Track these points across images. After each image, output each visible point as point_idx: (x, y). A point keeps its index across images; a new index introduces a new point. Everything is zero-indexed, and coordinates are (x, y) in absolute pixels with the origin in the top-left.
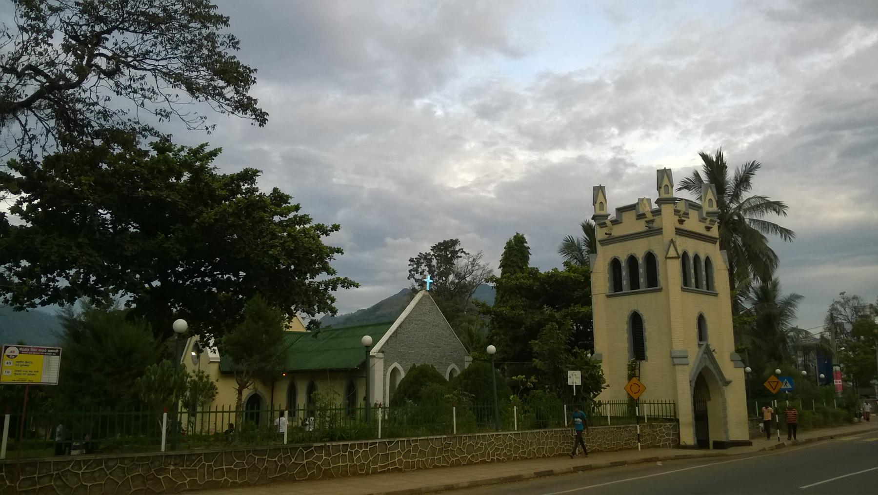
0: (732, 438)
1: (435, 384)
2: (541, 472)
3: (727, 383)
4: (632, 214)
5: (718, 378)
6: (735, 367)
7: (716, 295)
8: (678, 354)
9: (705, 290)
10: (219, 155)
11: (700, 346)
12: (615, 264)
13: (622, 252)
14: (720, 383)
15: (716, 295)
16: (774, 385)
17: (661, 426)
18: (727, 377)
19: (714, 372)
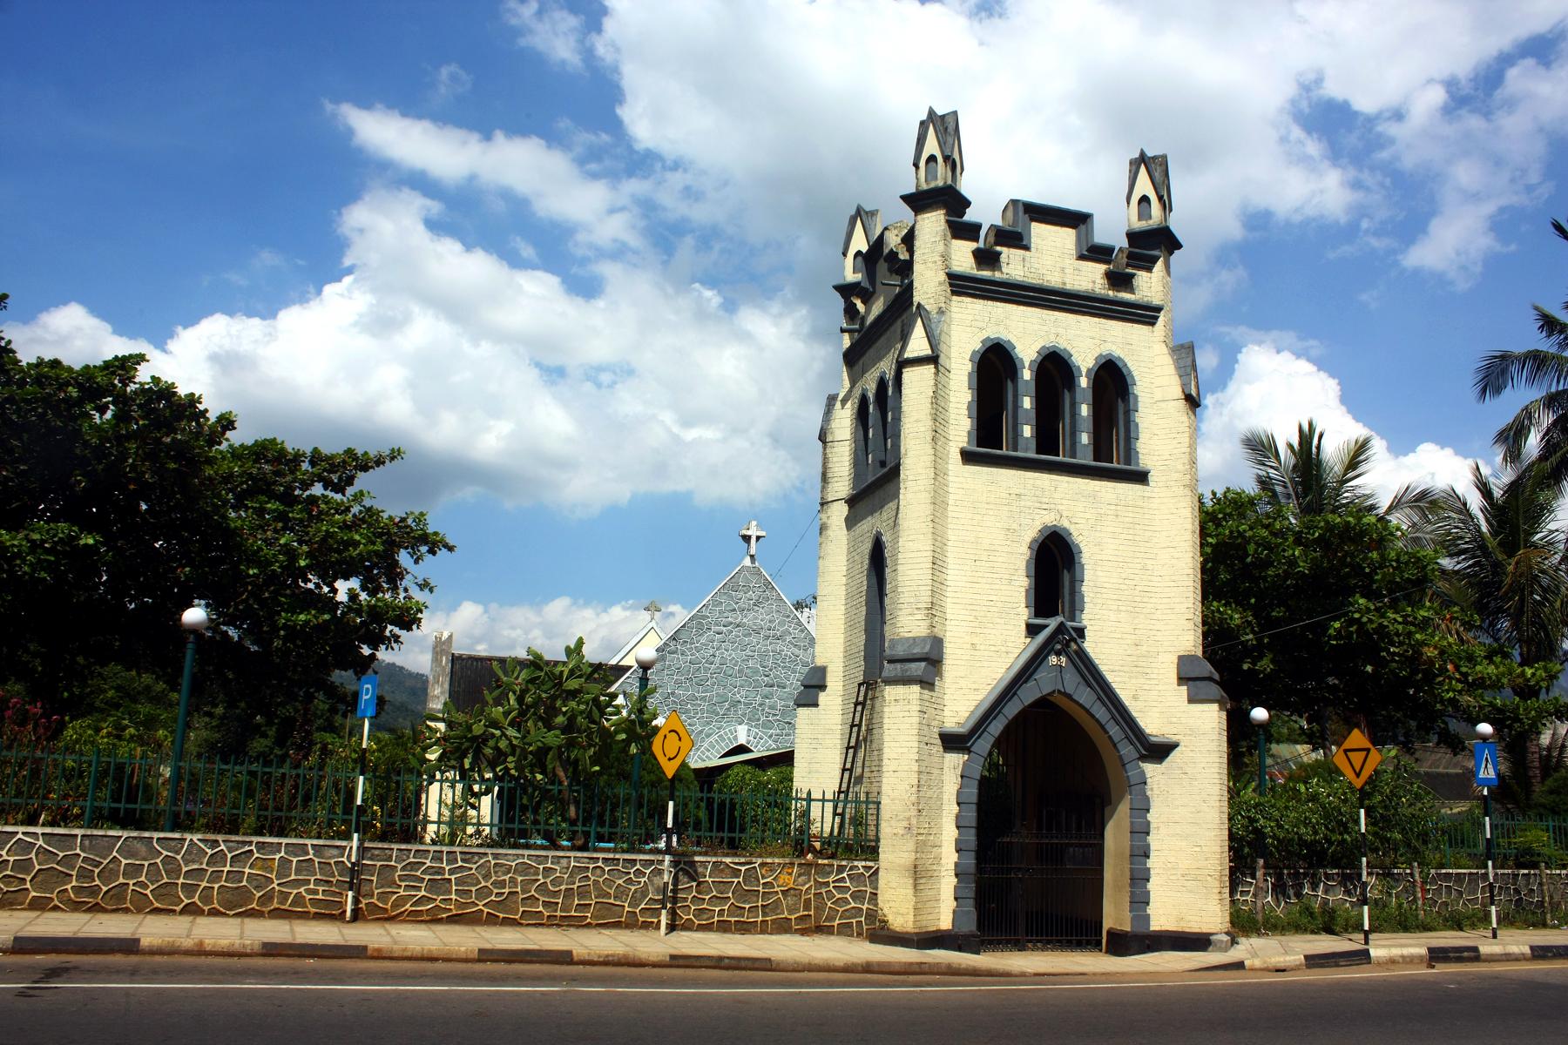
0: (1161, 918)
1: (1450, 567)
2: (491, 951)
3: (1160, 751)
4: (1065, 238)
5: (1114, 731)
6: (1191, 700)
7: (1141, 477)
8: (900, 651)
9: (1086, 459)
10: (1540, 305)
11: (1032, 630)
12: (994, 364)
13: (1029, 333)
14: (1127, 751)
15: (1141, 477)
16: (1357, 758)
17: (841, 869)
18: (1153, 724)
19: (1101, 713)
